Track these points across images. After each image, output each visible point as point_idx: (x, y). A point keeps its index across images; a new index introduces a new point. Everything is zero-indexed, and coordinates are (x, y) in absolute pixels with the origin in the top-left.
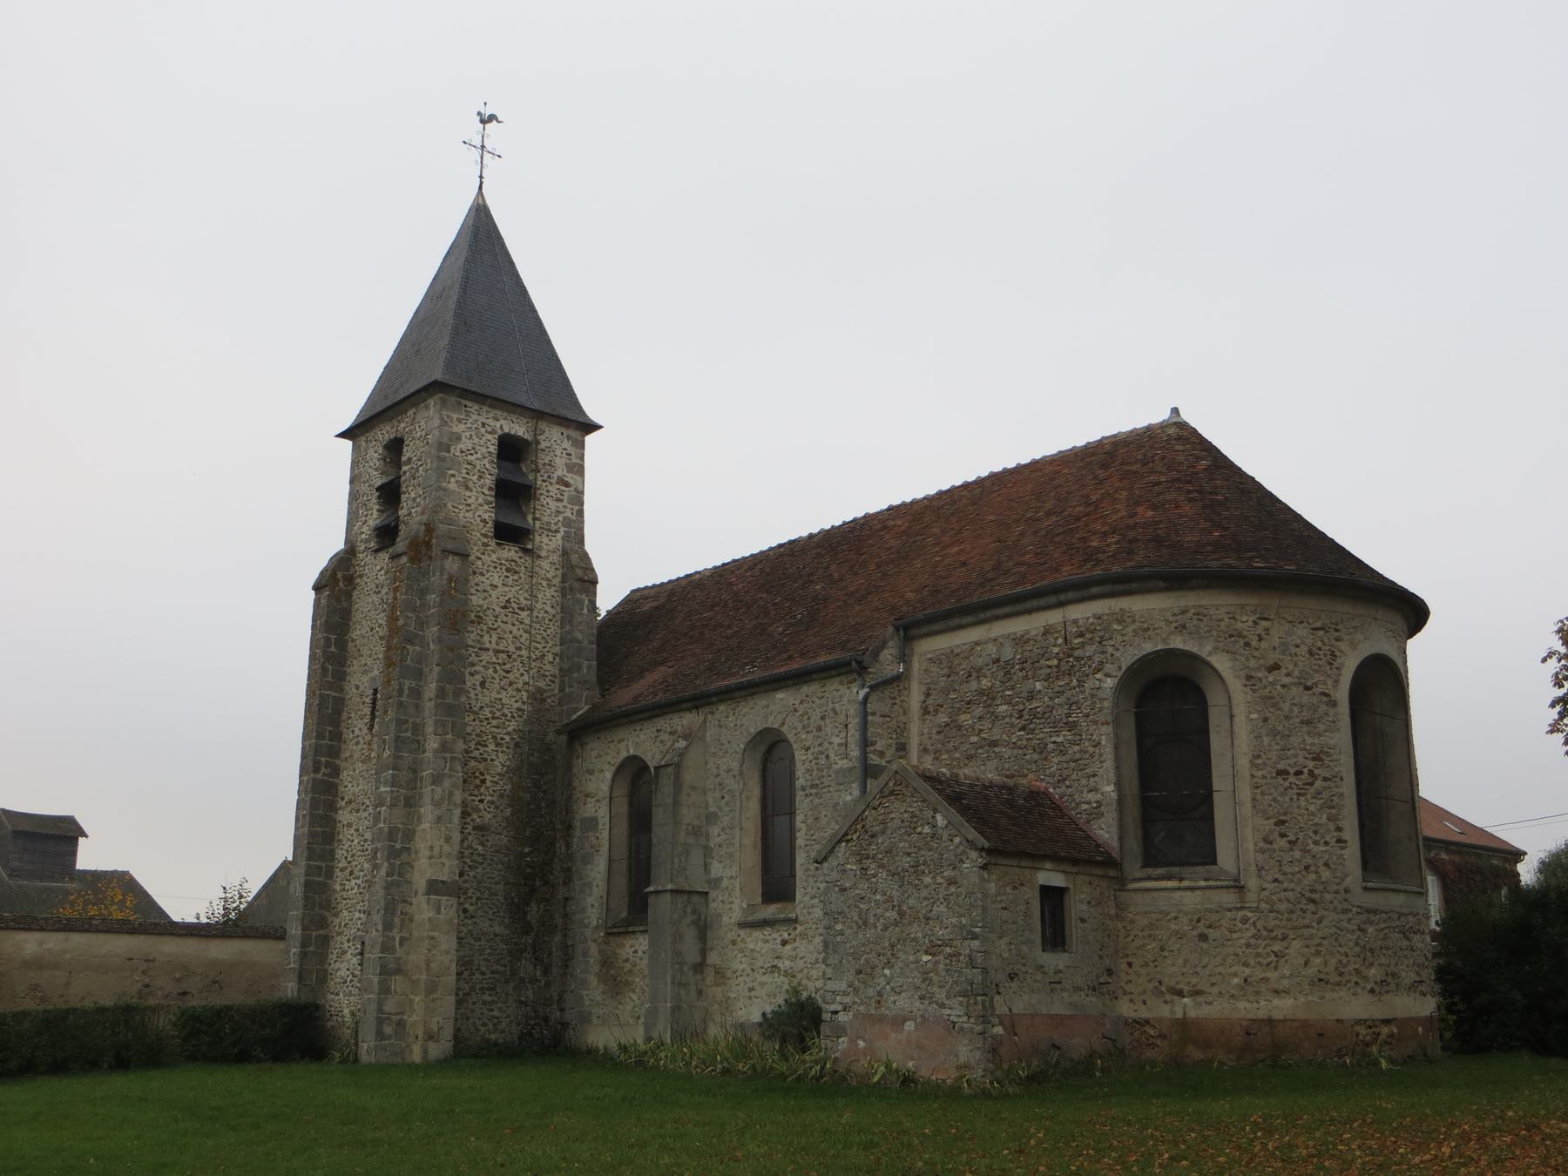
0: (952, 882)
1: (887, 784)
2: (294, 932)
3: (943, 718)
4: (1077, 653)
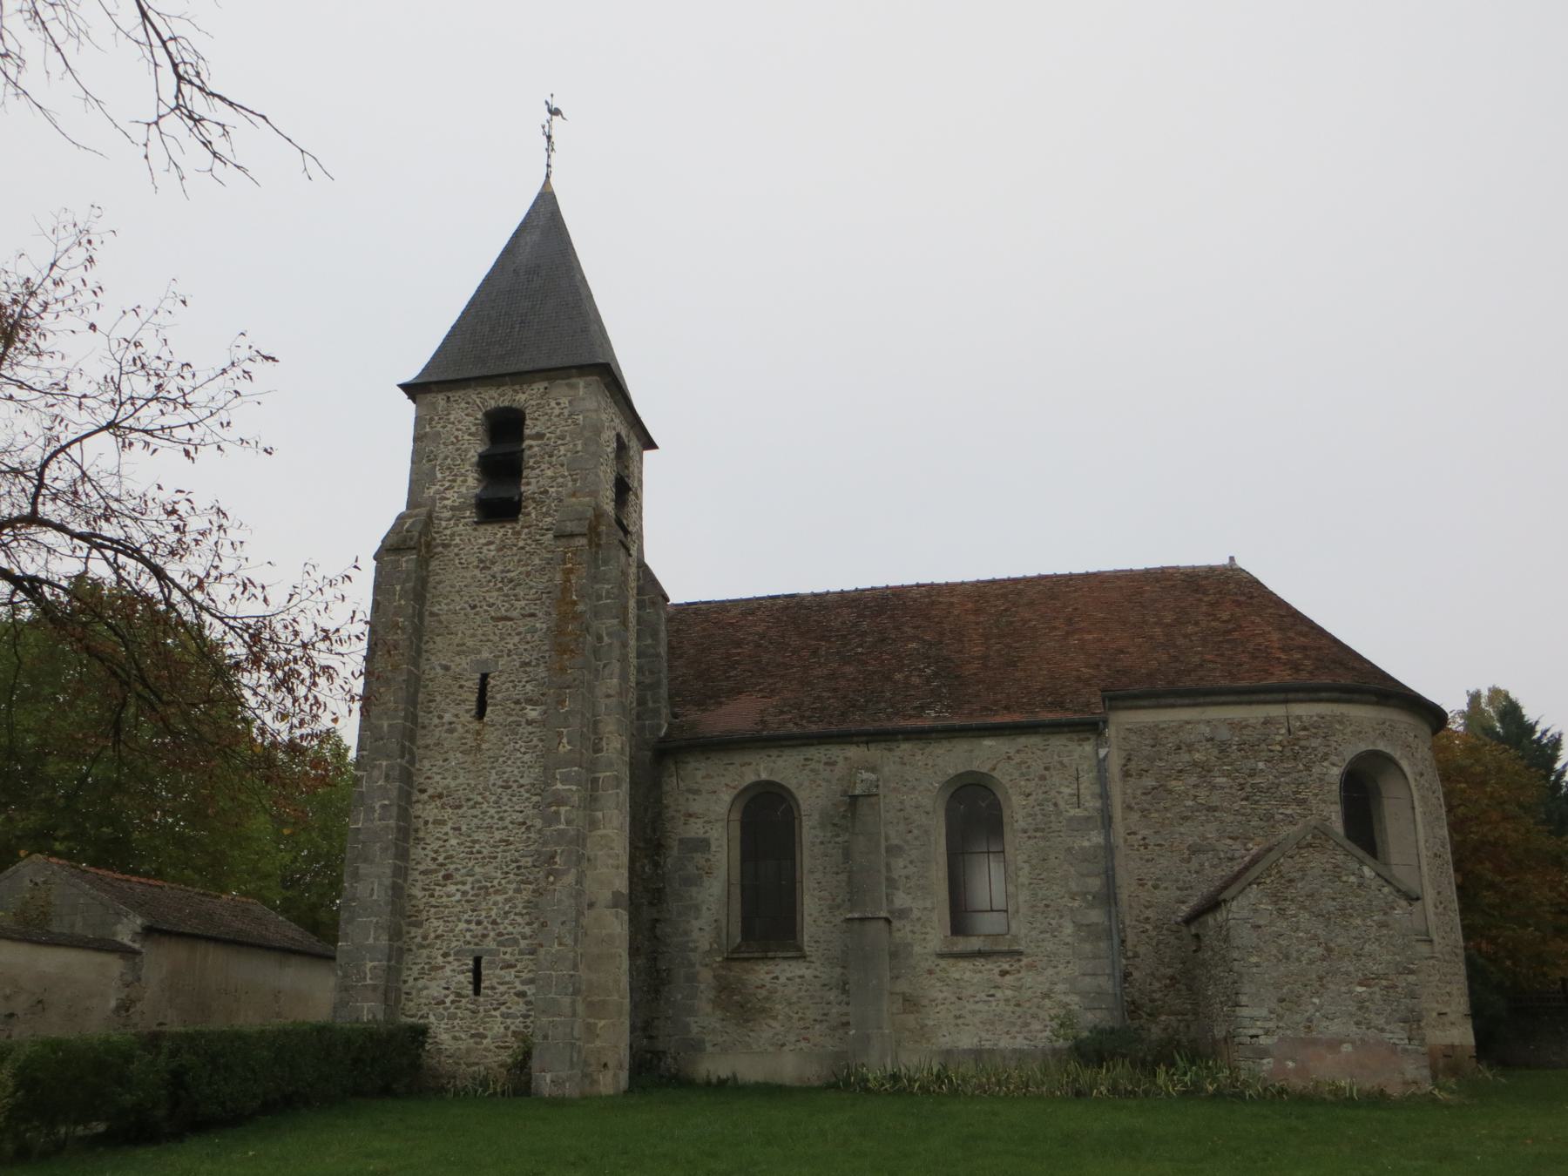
0: (1382, 925)
1: (1304, 837)
2: (371, 941)
3: (1149, 782)
4: (1303, 743)
